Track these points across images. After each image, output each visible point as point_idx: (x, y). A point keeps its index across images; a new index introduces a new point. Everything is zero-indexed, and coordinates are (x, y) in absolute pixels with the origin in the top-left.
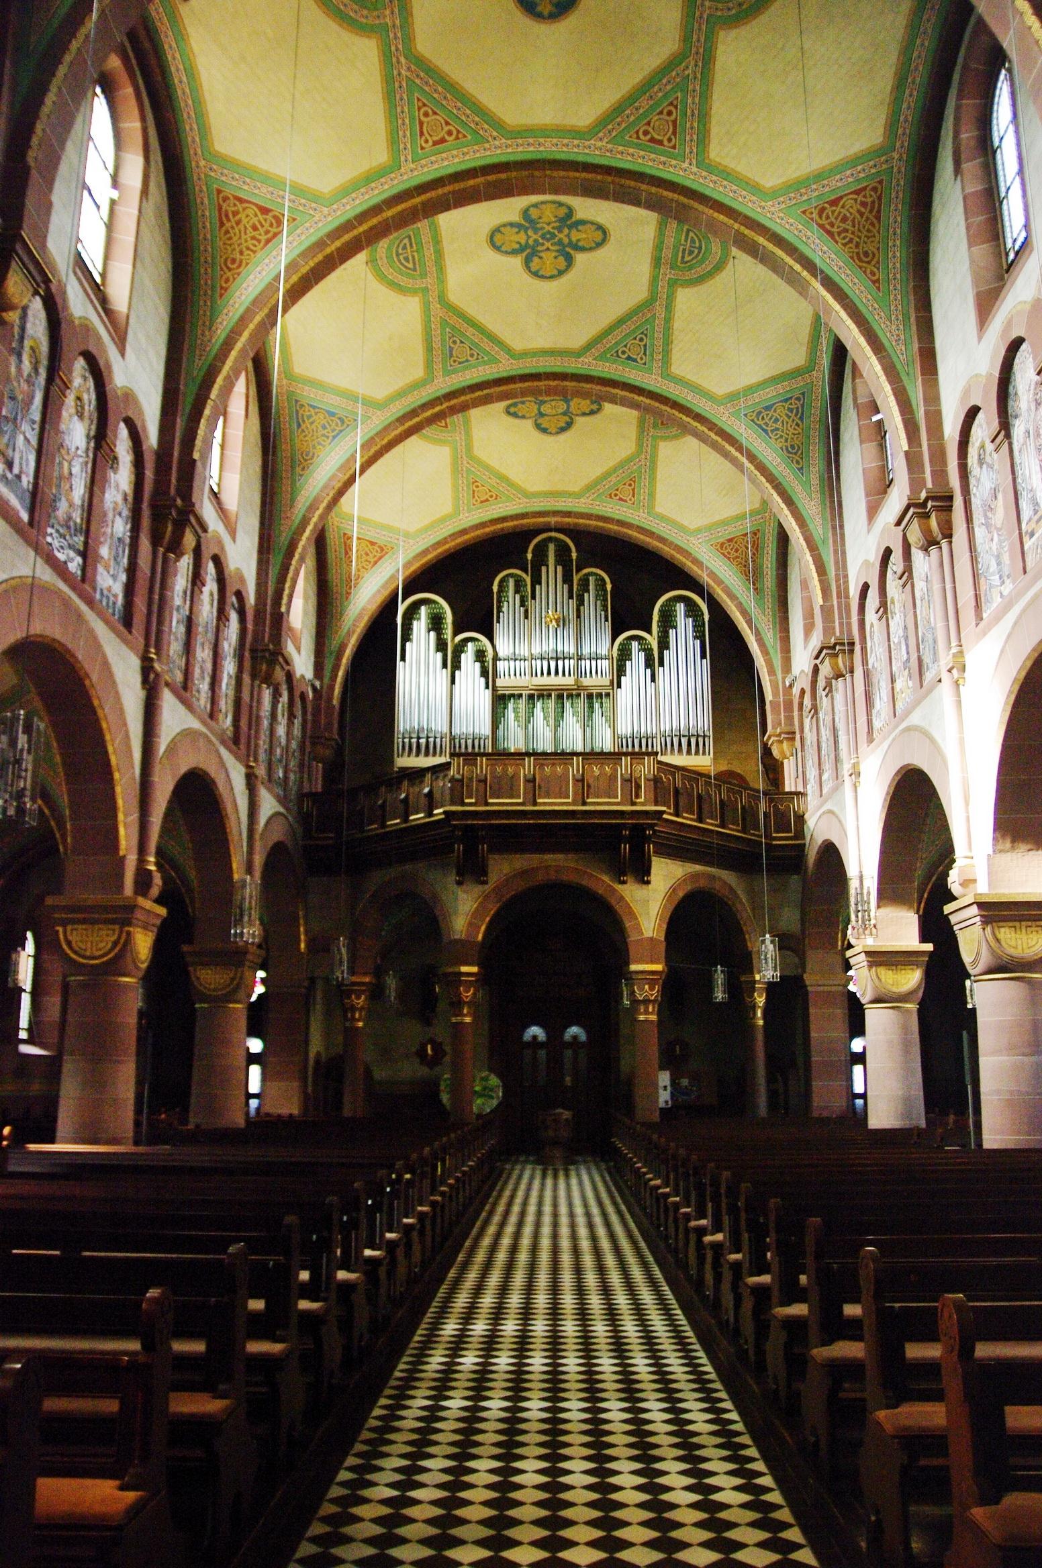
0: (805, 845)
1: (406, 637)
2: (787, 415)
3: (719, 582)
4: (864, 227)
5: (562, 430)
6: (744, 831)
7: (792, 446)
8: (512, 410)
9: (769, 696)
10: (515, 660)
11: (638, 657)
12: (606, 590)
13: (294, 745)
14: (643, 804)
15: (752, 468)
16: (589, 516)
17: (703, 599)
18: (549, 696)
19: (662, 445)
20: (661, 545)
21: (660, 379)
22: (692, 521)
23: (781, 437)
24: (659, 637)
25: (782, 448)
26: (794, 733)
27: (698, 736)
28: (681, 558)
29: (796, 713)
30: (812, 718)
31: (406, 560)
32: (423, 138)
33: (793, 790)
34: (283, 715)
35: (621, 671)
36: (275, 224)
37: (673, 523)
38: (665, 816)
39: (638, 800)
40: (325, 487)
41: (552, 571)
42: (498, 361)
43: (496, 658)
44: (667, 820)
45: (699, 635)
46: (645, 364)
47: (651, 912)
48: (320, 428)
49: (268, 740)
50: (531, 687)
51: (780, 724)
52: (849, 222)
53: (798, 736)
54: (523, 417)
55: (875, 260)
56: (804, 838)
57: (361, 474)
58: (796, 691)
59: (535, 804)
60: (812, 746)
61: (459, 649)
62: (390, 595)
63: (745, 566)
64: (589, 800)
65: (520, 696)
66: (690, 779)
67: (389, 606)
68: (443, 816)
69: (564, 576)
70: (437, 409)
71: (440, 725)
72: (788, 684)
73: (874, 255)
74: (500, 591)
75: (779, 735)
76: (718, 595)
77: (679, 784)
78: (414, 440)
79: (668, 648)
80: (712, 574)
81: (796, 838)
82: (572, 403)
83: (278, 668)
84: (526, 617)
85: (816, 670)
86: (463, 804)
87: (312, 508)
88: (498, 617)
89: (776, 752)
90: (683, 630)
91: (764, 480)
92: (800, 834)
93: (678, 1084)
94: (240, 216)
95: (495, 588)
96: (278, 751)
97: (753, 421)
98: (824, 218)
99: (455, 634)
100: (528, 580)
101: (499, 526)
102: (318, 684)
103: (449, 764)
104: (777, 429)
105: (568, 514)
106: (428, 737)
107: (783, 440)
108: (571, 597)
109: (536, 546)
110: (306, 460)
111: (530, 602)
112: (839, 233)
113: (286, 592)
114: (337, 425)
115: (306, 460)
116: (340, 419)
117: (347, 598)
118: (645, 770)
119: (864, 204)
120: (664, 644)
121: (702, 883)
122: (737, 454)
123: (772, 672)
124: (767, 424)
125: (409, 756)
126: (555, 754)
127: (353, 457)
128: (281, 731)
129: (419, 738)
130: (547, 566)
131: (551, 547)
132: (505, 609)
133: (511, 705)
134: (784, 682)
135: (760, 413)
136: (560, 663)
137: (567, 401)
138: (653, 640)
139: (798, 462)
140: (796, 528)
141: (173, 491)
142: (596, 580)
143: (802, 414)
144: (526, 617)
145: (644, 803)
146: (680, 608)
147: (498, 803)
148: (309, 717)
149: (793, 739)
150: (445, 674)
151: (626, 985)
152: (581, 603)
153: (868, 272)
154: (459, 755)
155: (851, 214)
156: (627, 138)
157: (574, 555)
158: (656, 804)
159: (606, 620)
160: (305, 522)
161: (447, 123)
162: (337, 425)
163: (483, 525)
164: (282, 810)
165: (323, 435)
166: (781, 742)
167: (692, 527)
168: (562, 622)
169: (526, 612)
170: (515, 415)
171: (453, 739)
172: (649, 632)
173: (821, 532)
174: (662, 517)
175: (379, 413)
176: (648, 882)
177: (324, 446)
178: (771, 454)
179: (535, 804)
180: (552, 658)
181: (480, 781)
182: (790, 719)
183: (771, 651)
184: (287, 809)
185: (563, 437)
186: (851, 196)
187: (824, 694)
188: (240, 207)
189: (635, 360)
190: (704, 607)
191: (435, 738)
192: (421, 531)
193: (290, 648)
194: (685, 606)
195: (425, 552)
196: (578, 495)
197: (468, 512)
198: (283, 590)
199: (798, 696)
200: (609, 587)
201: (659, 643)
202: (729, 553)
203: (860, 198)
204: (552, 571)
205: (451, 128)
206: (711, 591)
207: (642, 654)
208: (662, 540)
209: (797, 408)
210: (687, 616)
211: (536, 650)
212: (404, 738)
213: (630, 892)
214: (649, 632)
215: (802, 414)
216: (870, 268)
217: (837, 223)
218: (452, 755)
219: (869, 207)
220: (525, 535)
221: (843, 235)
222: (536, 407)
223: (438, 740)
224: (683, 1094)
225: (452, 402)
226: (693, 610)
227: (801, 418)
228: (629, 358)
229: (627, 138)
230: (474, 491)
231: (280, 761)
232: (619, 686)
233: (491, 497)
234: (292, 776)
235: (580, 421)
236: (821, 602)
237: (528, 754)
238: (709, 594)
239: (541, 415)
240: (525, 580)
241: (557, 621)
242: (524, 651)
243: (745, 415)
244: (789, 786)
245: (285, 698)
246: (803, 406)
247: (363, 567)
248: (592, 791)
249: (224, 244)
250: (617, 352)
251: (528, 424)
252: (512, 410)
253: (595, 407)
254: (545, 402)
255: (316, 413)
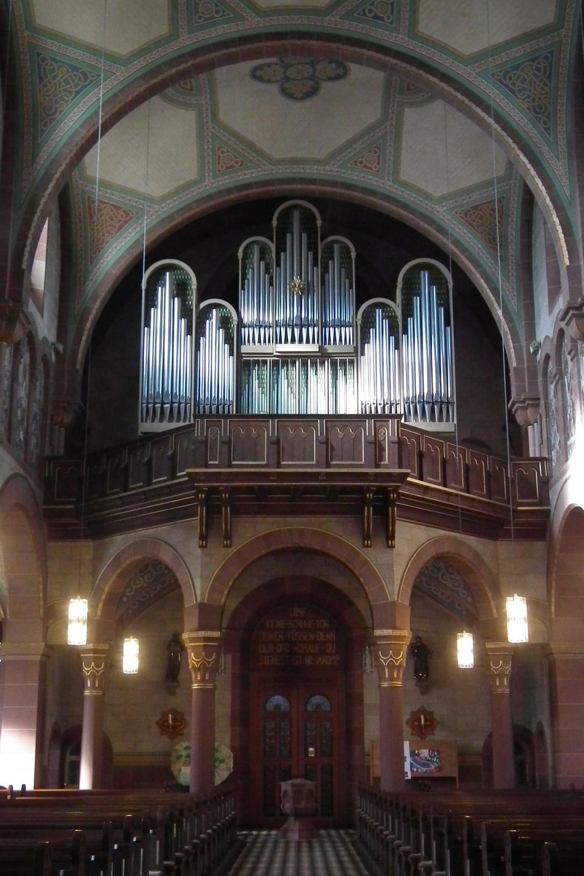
0: (550, 510)
1: (151, 302)
2: (535, 75)
3: (464, 250)
4: (539, 85)
5: (308, 95)
6: (489, 496)
7: (540, 107)
8: (258, 73)
9: (513, 364)
10: (260, 327)
11: (381, 325)
12: (350, 258)
13: (35, 408)
14: (386, 466)
15: (499, 129)
16: (334, 184)
17: (448, 267)
18: (294, 363)
19: (407, 111)
20: (405, 213)
21: (407, 39)
22: (437, 189)
23: (529, 97)
24: (403, 304)
25: (529, 109)
26: (539, 399)
27: (442, 402)
28: (426, 225)
29: (540, 379)
30: (557, 383)
31: (150, 226)
32: (220, 165)
33: (537, 455)
34: (25, 377)
35: (365, 339)
36: (83, 79)
37: (420, 192)
38: (409, 479)
39: (382, 463)
40: (66, 144)
41: (296, 239)
42: (244, 19)
43: (241, 324)
44: (411, 484)
45: (443, 302)
46: (391, 23)
47: (396, 577)
48: (63, 84)
49: (8, 401)
50: (275, 354)
51: (524, 391)
52: (527, 82)
53: (542, 402)
54: (269, 81)
55: (547, 113)
56: (549, 504)
57: (102, 135)
58: (540, 357)
59: (279, 465)
60: (557, 411)
61: (204, 315)
62: (134, 260)
63: (489, 234)
64: (333, 463)
65: (265, 362)
66: (434, 443)
67: (133, 273)
68: (186, 479)
69: (309, 244)
70: (182, 67)
71: (184, 389)
72: (532, 350)
73: (546, 108)
74: (244, 258)
75: (524, 401)
76: (462, 262)
77: (424, 448)
78: (156, 99)
79: (412, 316)
80: (456, 242)
81: (540, 503)
82: (318, 67)
83: (18, 326)
84: (271, 284)
85: (561, 334)
86: (207, 466)
87: (54, 163)
88: (243, 285)
89: (519, 419)
90: (427, 291)
91: (510, 141)
92: (545, 500)
93: (418, 755)
94: (102, 212)
95: (240, 255)
96: (19, 413)
97: (500, 80)
98: (469, 217)
99: (200, 300)
100: (273, 246)
101: (245, 193)
102: (61, 348)
103: (193, 425)
104: (524, 89)
105: (313, 181)
106: (172, 403)
107: (530, 100)
108: (315, 264)
109: (281, 213)
110: (48, 116)
111: (274, 269)
112: (520, 91)
113: (27, 249)
114: (80, 80)
115: (48, 116)
116: (83, 73)
117: (91, 262)
118: (389, 432)
119: (538, 69)
120: (408, 312)
121: (447, 548)
122: (486, 116)
123: (516, 339)
124: (514, 84)
125: (153, 421)
126: (299, 416)
127: (96, 112)
128: (22, 392)
129: (163, 403)
130: (293, 234)
131: (296, 215)
132: (249, 276)
133: (255, 373)
134: (528, 350)
135: (507, 72)
136: (304, 331)
137: (313, 64)
138: (397, 308)
139: (545, 123)
140: (543, 189)
141: (7, 296)
142: (341, 247)
143: (550, 74)
144: (271, 284)
145: (389, 465)
146: (425, 276)
147: (243, 465)
148: (52, 381)
149: (538, 405)
150: (187, 343)
151: (370, 651)
152: (325, 270)
153: (542, 121)
154: (204, 416)
155: (485, 215)
156: (355, 15)
157: (319, 223)
158: (400, 467)
159: (351, 287)
160: (47, 177)
161: (236, 157)
162: (80, 80)
163: (229, 191)
164: (22, 472)
165: (111, 225)
166: (526, 408)
167: (438, 194)
168: (307, 290)
169: (271, 279)
170: (260, 79)
171: (197, 404)
172: (393, 299)
173: (568, 193)
174: (406, 185)
175: (123, 69)
176: (393, 547)
177: (67, 102)
178: (518, 116)
179: (279, 465)
180: (296, 325)
181: (224, 443)
182: (534, 385)
183: (515, 318)
184: (24, 469)
185: (308, 103)
186: (529, 63)
187: (569, 357)
188: (102, 206)
189: (382, 19)
190: (448, 276)
191: (180, 403)
192: (165, 198)
193: (32, 308)
194: (429, 274)
195: (170, 217)
196: (324, 162)
197: (214, 178)
198: (24, 246)
199: (542, 362)
200: (353, 255)
201: (403, 310)
202: (474, 221)
203: (535, 64)
204: (296, 239)
205: (238, 159)
206: (455, 260)
207: (386, 323)
208: (406, 207)
209: (545, 67)
210: (431, 284)
211: (281, 317)
212: (148, 403)
213: (375, 556)
214: (393, 299)
215: (550, 74)
216: (543, 118)
217: (477, 220)
218: (195, 417)
219: (542, 72)
220: (274, 201)
221: (523, 92)
222: (281, 70)
223: (182, 406)
224: (424, 765)
225: (198, 60)
226: (437, 279)
227: (549, 78)
228: (376, 17)
229: (355, 15)
230: (219, 158)
231: (21, 422)
232: (363, 354)
233: (237, 163)
234: (33, 440)
235: (326, 86)
236: (567, 262)
237: (272, 416)
238: (453, 262)
239: (288, 79)
240: (270, 248)
241: (302, 290)
242: (269, 319)
243: (493, 75)
244: (533, 451)
245: (26, 359)
246: (551, 65)
247: (108, 232)
248: (335, 453)
249: (44, 95)
250: (364, 10)
251: (274, 88)
252: (258, 73)
253: (341, 71)
254: (292, 65)
255: (59, 67)
